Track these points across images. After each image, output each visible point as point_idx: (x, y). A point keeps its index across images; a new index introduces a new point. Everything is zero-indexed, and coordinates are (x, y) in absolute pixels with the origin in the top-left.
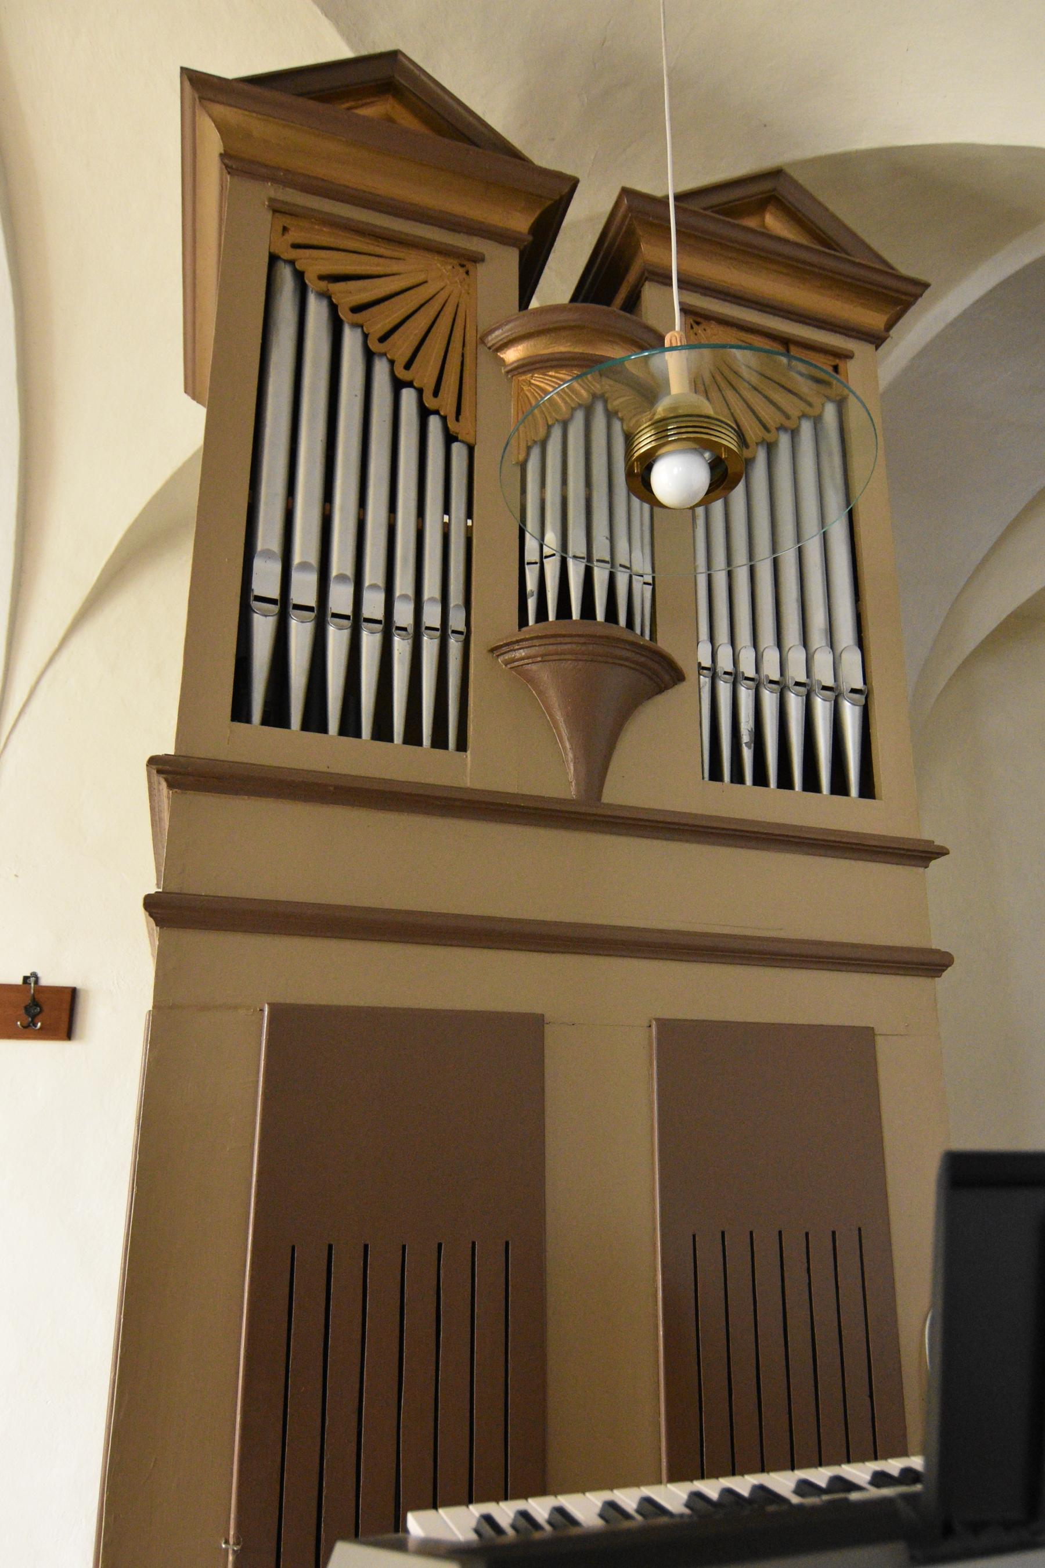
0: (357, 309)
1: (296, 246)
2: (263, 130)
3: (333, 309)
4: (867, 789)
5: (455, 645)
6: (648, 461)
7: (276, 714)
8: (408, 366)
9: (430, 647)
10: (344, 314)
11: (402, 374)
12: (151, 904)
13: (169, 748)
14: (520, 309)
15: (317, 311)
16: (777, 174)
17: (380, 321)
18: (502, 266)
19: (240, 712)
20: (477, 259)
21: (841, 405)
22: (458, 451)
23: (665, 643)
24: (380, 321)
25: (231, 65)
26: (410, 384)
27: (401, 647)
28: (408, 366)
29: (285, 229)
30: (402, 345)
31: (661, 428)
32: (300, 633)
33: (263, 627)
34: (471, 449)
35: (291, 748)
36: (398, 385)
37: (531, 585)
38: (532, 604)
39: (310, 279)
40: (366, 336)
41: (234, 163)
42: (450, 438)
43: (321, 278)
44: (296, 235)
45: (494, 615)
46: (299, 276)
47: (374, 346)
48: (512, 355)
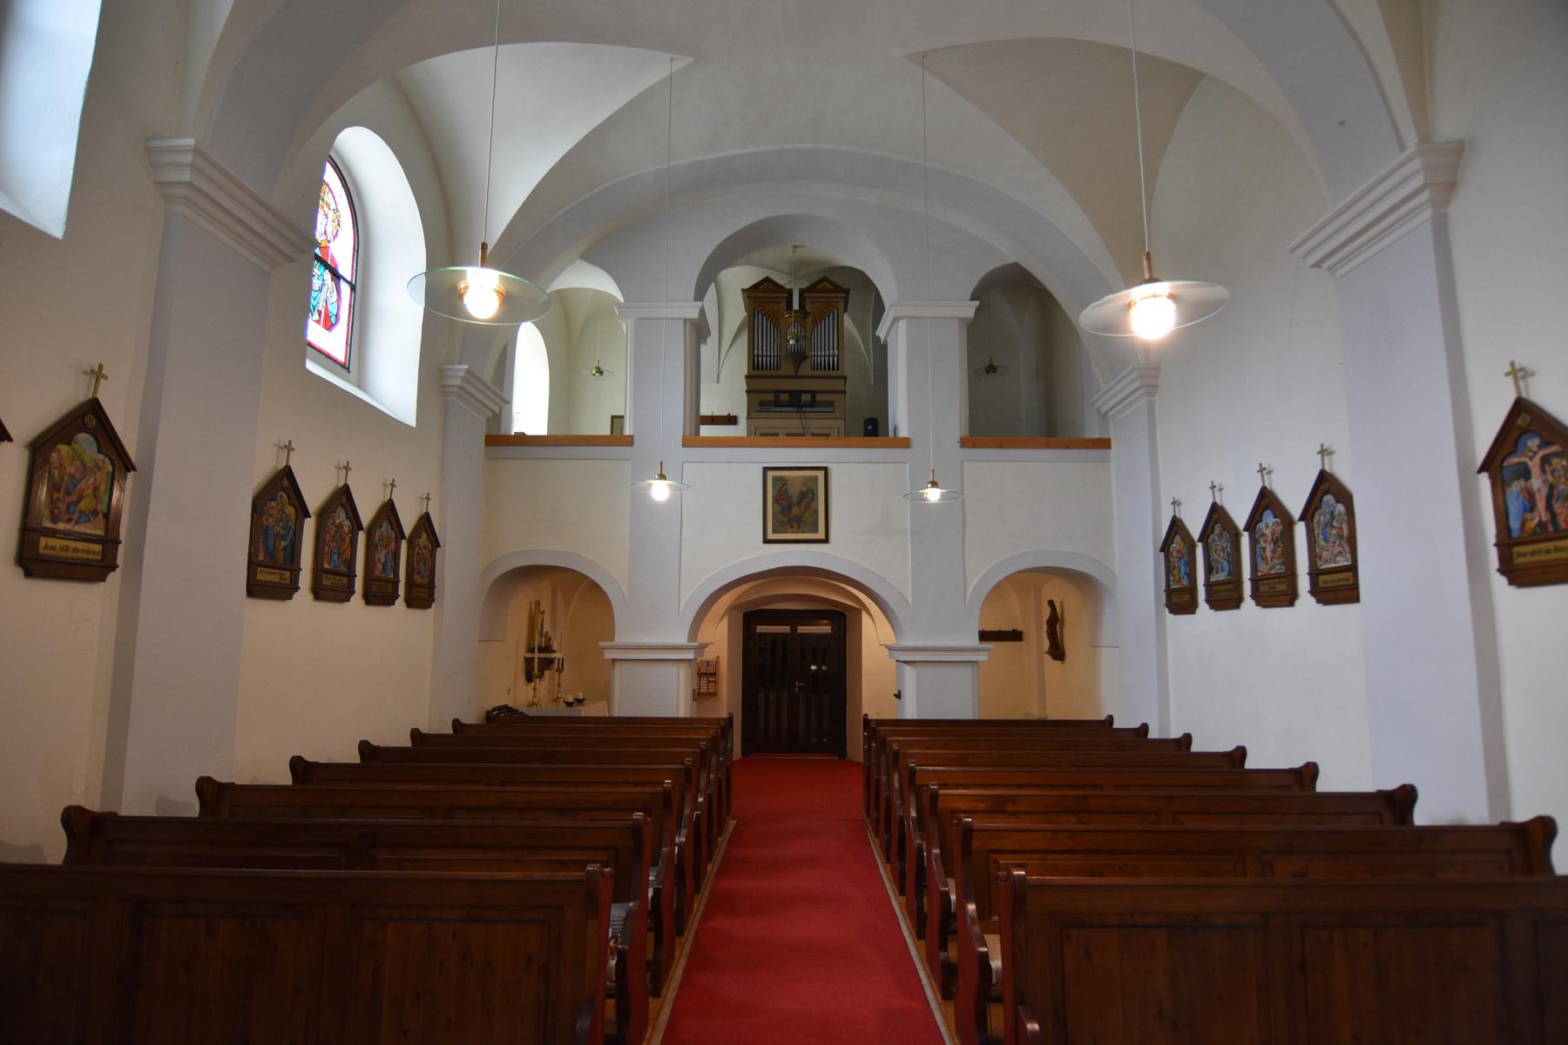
18: (783, 305)
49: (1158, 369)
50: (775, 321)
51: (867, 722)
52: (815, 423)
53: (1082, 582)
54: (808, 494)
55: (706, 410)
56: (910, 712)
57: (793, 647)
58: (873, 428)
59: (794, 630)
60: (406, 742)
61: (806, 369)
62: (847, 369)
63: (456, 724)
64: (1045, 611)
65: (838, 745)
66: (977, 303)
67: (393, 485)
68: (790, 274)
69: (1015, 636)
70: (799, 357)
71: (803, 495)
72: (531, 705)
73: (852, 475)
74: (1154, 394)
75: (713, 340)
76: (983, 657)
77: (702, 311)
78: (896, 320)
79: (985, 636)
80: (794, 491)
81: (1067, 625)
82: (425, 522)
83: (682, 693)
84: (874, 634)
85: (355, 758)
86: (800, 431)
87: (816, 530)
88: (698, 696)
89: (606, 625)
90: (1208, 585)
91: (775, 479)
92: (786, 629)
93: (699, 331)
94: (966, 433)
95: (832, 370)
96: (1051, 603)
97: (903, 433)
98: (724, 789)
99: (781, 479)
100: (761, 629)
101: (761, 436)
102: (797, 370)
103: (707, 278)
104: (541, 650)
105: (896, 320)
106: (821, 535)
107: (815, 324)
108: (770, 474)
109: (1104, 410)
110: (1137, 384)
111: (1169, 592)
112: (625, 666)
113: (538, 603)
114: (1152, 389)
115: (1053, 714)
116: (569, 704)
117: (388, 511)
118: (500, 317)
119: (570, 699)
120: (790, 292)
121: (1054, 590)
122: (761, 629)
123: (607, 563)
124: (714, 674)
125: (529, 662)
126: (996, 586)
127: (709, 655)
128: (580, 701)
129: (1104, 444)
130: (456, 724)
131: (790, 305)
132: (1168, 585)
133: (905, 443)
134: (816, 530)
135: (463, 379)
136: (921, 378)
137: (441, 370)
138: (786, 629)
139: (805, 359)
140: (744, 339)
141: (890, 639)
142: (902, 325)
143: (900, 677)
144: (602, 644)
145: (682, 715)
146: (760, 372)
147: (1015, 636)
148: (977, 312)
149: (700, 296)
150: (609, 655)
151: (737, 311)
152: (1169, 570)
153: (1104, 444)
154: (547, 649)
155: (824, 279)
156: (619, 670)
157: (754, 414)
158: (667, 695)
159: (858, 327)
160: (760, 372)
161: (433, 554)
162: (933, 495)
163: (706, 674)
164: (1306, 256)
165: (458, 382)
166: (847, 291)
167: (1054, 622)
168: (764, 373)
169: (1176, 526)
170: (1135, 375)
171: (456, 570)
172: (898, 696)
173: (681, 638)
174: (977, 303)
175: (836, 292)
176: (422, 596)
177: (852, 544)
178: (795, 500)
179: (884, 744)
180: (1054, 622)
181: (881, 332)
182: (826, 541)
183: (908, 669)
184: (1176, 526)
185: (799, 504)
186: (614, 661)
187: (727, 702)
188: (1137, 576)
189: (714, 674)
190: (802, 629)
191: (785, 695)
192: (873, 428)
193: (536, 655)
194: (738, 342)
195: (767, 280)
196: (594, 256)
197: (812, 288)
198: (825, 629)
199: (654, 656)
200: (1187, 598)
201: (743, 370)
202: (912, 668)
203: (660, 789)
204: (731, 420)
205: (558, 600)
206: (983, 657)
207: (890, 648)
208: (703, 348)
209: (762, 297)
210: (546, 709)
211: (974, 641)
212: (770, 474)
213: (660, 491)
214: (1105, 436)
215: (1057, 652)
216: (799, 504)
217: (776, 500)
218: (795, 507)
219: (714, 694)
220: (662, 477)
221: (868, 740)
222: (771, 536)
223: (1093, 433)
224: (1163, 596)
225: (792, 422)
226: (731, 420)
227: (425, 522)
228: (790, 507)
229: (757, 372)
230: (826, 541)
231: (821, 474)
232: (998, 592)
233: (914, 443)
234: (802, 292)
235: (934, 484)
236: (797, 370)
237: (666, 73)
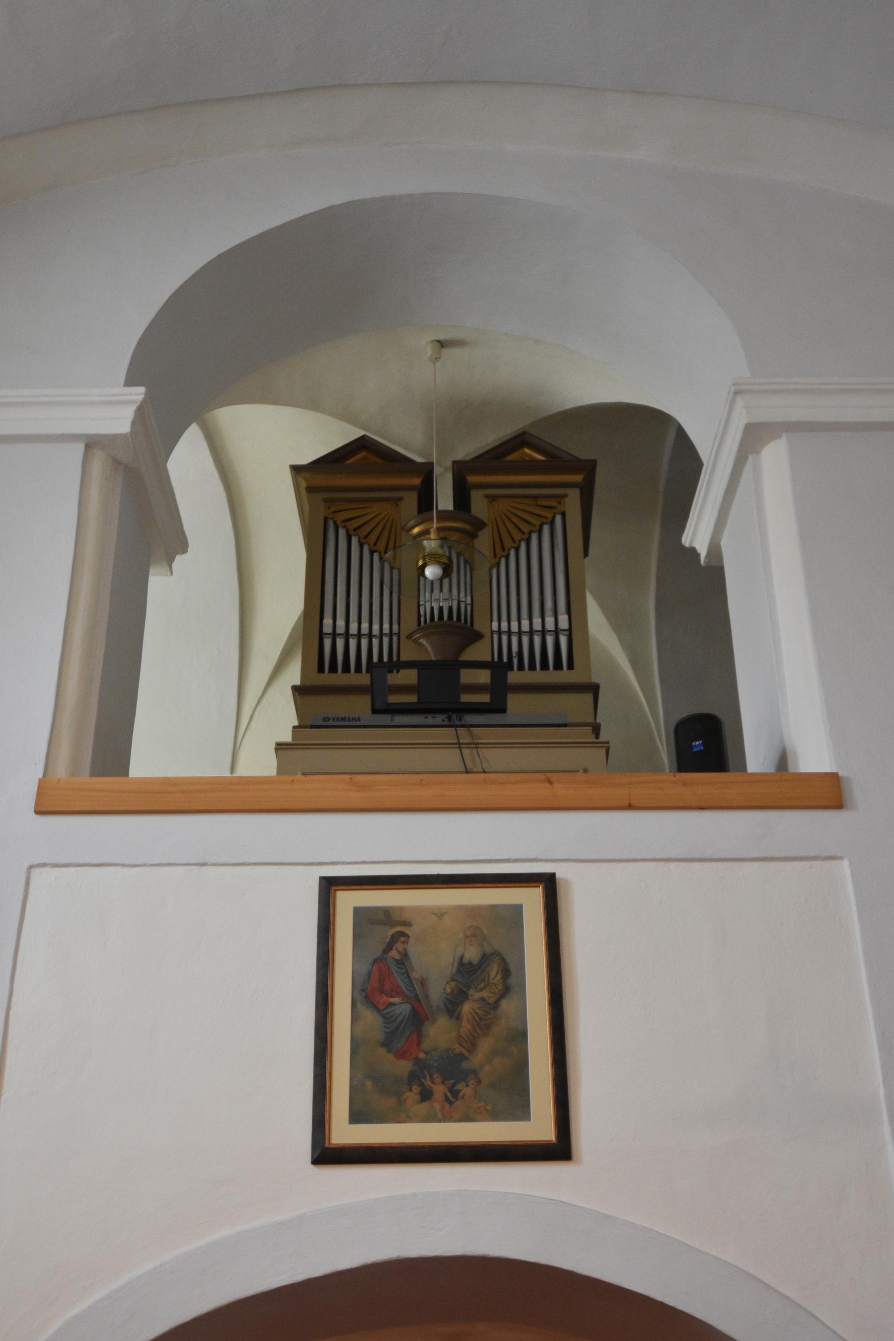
0: (355, 530)
1: (334, 512)
2: (321, 480)
3: (347, 531)
4: (571, 666)
5: (395, 638)
6: (424, 566)
7: (333, 669)
8: (375, 545)
9: (386, 640)
10: (351, 532)
11: (374, 549)
12: (295, 689)
13: (298, 683)
14: (420, 511)
15: (342, 533)
16: (523, 434)
17: (364, 532)
18: (411, 501)
19: (321, 669)
20: (400, 499)
21: (563, 515)
22: (395, 572)
23: (477, 626)
24: (364, 532)
25: (306, 459)
26: (376, 551)
27: (375, 642)
28: (375, 545)
29: (329, 508)
30: (373, 537)
31: (424, 558)
32: (340, 643)
33: (327, 643)
34: (400, 571)
35: (340, 679)
36: (372, 552)
37: (422, 612)
38: (422, 619)
39: (339, 523)
40: (359, 538)
41: (310, 490)
42: (392, 568)
43: (343, 521)
44: (333, 509)
45: (409, 624)
46: (335, 522)
47: (363, 541)
48: (416, 530)
50: (384, 541)
54: (487, 972)
71: (468, 973)
73: (643, 908)
80: (434, 963)
97: (814, 758)
99: (385, 916)
106: (539, 1127)
107: (500, 551)
108: (347, 902)
120: (427, 472)
131: (426, 501)
133: (827, 793)
134: (519, 1108)
142: (774, 457)
155: (520, 440)
166: (589, 469)
168: (352, 723)
178: (437, 992)
181: (697, 535)
185: (452, 1006)
194: (271, 691)
208: (159, 585)
209: (352, 493)
216: (452, 1006)
217: (367, 993)
218: (438, 1030)
222: (344, 1132)
225: (430, 749)
228: (419, 1018)
230: (559, 1150)
231: (531, 900)
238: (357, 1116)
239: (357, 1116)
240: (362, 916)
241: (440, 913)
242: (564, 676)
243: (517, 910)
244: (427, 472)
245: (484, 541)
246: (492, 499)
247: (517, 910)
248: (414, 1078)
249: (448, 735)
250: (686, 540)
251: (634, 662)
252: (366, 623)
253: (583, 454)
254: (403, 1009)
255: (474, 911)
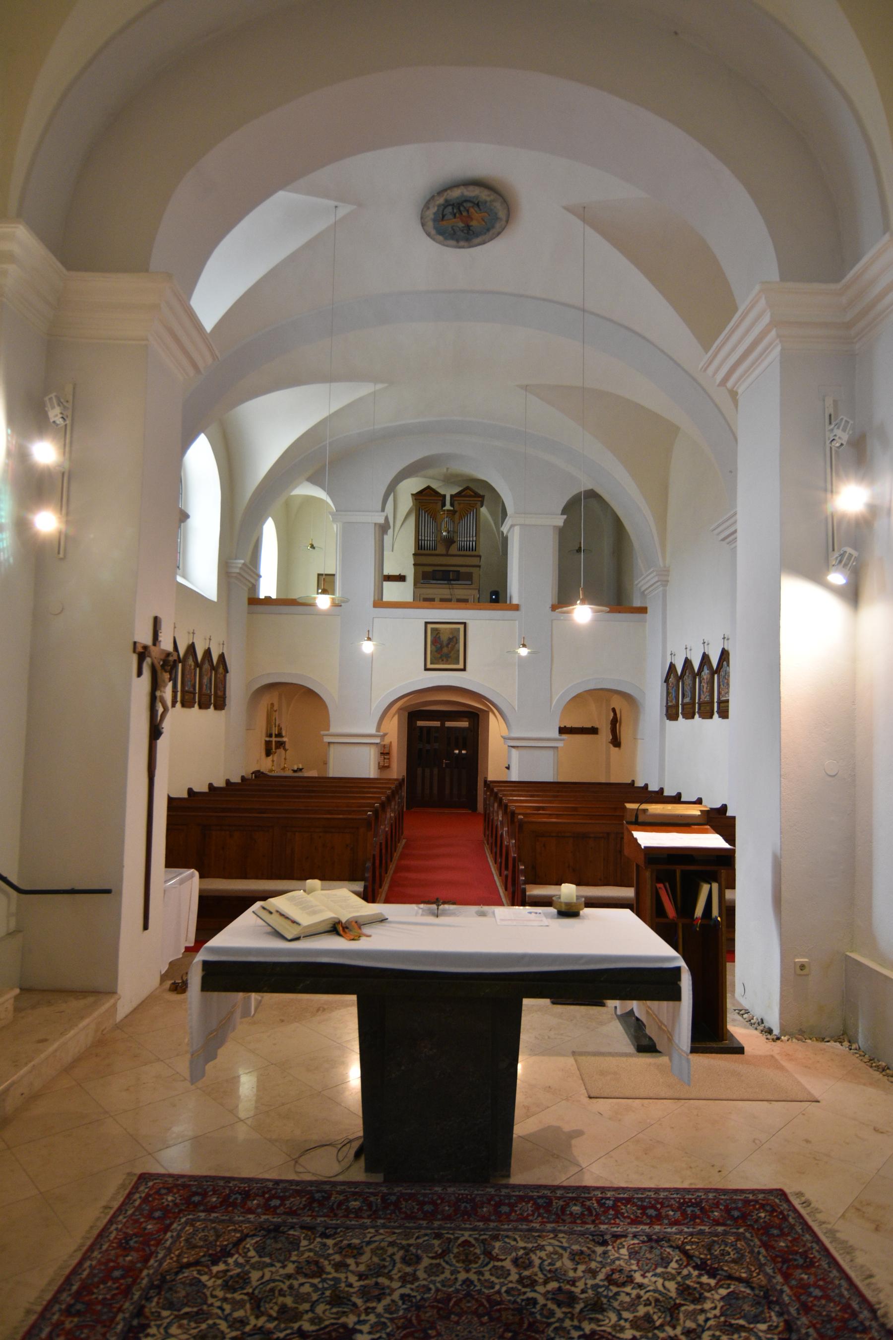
18: (440, 504)
49: (668, 571)
50: (434, 516)
51: (487, 784)
52: (460, 592)
53: (627, 697)
54: (453, 640)
55: (386, 572)
56: (514, 776)
57: (442, 737)
58: (497, 597)
59: (443, 724)
60: (185, 795)
61: (453, 550)
62: (483, 550)
63: (211, 786)
64: (604, 719)
65: (472, 804)
66: (565, 517)
67: (193, 633)
68: (443, 481)
69: (593, 731)
70: (449, 542)
71: (450, 640)
72: (271, 771)
73: (482, 627)
74: (666, 585)
75: (390, 531)
76: (560, 744)
77: (387, 518)
78: (512, 526)
79: (563, 730)
80: (444, 638)
81: (623, 725)
82: (222, 657)
83: (372, 763)
84: (495, 728)
85: (185, 795)
86: (449, 597)
87: (458, 663)
88: (383, 768)
89: (325, 722)
90: (683, 705)
91: (432, 629)
92: (437, 724)
93: (383, 528)
94: (555, 602)
95: (471, 551)
96: (614, 710)
97: (515, 601)
98: (400, 818)
100: (420, 723)
101: (422, 600)
102: (447, 551)
103: (392, 488)
104: (276, 736)
105: (512, 526)
106: (461, 666)
107: (461, 518)
109: (643, 589)
110: (656, 579)
111: (668, 708)
112: (336, 746)
113: (272, 705)
114: (665, 583)
115: (613, 780)
116: (295, 771)
117: (208, 653)
118: (497, 791)
119: (295, 768)
120: (444, 496)
121: (616, 702)
122: (420, 723)
123: (326, 684)
124: (388, 754)
125: (268, 744)
126: (578, 696)
127: (387, 741)
128: (301, 770)
129: (643, 610)
130: (211, 786)
132: (667, 703)
133: (516, 608)
134: (458, 663)
135: (241, 568)
136: (528, 567)
137: (227, 563)
138: (437, 724)
139: (453, 548)
140: (412, 521)
141: (505, 732)
142: (517, 529)
143: (509, 757)
144: (322, 733)
145: (372, 776)
146: (423, 552)
147: (593, 731)
148: (565, 522)
149: (383, 510)
150: (327, 739)
151: (406, 503)
152: (668, 693)
153: (643, 610)
154: (279, 735)
155: (467, 488)
156: (333, 750)
157: (419, 585)
158: (363, 765)
159: (492, 514)
160: (423, 552)
161: (225, 676)
162: (523, 652)
163: (385, 753)
164: (719, 534)
165: (237, 571)
166: (483, 497)
167: (615, 722)
169: (672, 667)
170: (655, 573)
171: (237, 687)
172: (508, 768)
173: (373, 731)
174: (565, 517)
175: (474, 495)
176: (220, 705)
177: (477, 675)
178: (445, 643)
179: (492, 790)
180: (615, 722)
181: (505, 529)
182: (464, 669)
183: (514, 751)
184: (672, 667)
185: (447, 645)
186: (329, 743)
187: (397, 770)
188: (654, 698)
189: (388, 754)
190: (448, 724)
191: (436, 771)
192: (497, 597)
193: (274, 739)
195: (429, 488)
196: (315, 479)
197: (459, 494)
198: (464, 724)
199: (354, 741)
200: (674, 711)
201: (411, 548)
202: (519, 751)
203: (365, 817)
204: (401, 578)
205: (292, 703)
206: (560, 744)
207: (504, 738)
208: (385, 537)
209: (426, 500)
210: (278, 773)
211: (555, 734)
212: (430, 626)
213: (368, 647)
214: (643, 605)
215: (616, 742)
216: (447, 645)
217: (434, 642)
218: (445, 648)
219: (388, 767)
220: (369, 639)
221: (485, 793)
222: (429, 666)
223: (637, 603)
224: (665, 709)
226: (401, 578)
227: (222, 657)
228: (442, 647)
229: (421, 551)
230: (464, 669)
231: (461, 627)
232: (579, 700)
233: (522, 608)
234: (452, 496)
235: (524, 646)
236: (447, 551)
237: (332, 221)
238: (431, 663)
239: (431, 663)
240: (432, 629)
241: (446, 629)
242: (474, 553)
243: (459, 629)
244: (444, 496)
245: (457, 516)
246: (459, 504)
247: (459, 629)
248: (441, 658)
249: (447, 586)
250: (502, 529)
251: (494, 520)
252: (429, 538)
253: (481, 494)
254: (439, 646)
255: (451, 629)
